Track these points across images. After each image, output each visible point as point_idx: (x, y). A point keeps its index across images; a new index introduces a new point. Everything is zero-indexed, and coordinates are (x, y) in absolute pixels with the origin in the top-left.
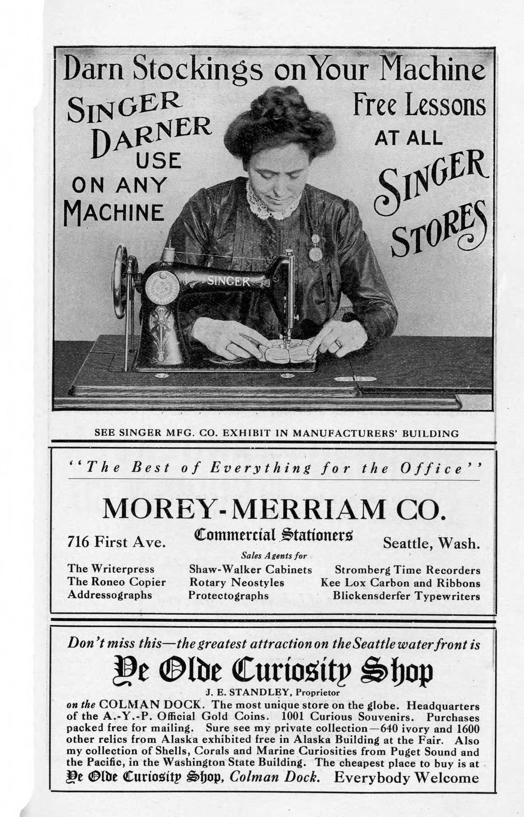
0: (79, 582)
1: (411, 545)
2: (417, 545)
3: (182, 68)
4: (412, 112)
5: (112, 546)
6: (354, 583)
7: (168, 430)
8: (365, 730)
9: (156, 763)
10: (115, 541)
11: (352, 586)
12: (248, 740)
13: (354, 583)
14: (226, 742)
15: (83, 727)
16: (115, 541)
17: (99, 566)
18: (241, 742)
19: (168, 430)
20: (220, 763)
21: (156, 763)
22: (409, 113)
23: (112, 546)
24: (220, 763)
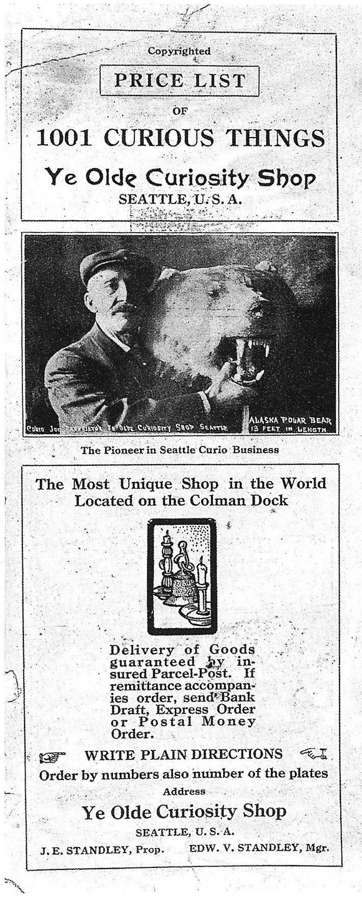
0: (51, 485)
1: (182, 451)
2: (186, 451)
3: (275, 500)
4: (80, 504)
5: (181, 184)
6: (87, 502)
7: (76, 480)
8: (152, 503)
9: (181, 502)
10: (151, 773)
11: (84, 505)
12: (128, 502)
13: (87, 502)
14: (100, 853)
15: (277, 500)
16: (151, 773)
17: (292, 480)
18: (119, 505)
19: (76, 480)
20: (150, 502)
21: (181, 502)
22: (78, 505)
23: (181, 184)
24: (150, 502)
